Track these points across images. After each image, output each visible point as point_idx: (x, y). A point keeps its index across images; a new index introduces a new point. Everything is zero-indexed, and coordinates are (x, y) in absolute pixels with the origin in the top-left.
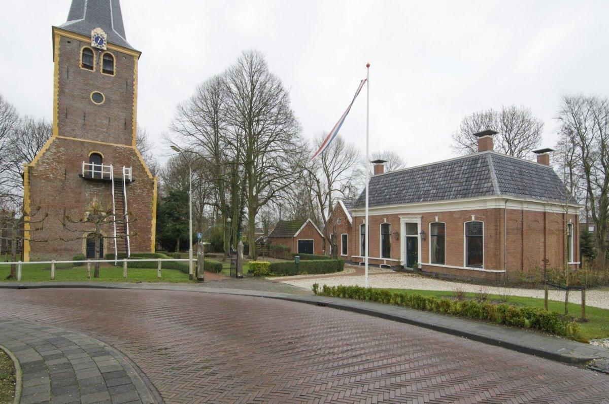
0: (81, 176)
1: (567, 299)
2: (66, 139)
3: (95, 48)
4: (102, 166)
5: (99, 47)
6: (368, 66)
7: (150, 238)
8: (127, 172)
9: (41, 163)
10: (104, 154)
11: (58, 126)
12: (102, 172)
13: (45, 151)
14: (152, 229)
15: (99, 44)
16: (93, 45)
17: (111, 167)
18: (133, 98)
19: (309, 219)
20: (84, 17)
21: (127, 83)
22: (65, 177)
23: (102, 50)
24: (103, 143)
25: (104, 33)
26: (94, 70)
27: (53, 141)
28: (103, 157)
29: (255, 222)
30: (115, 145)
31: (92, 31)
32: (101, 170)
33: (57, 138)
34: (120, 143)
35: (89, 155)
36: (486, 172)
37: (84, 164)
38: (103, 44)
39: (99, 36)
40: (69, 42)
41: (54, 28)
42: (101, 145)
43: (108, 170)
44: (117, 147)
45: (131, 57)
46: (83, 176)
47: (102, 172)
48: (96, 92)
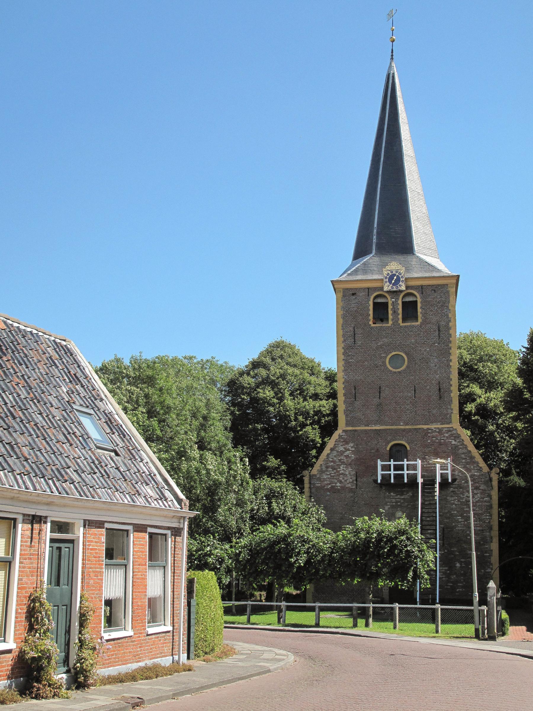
0: (376, 481)
2: (356, 431)
4: (405, 463)
5: (395, 289)
6: (390, 15)
8: (443, 467)
10: (409, 443)
13: (329, 452)
14: (492, 558)
15: (394, 284)
17: (419, 462)
21: (439, 327)
23: (401, 291)
24: (407, 427)
25: (400, 267)
26: (390, 322)
28: (408, 448)
29: (489, 586)
30: (425, 427)
32: (403, 470)
33: (343, 431)
35: (388, 449)
36: (300, 418)
37: (379, 463)
38: (401, 283)
41: (332, 282)
42: (404, 430)
43: (415, 468)
44: (428, 429)
46: (379, 481)
47: (406, 472)
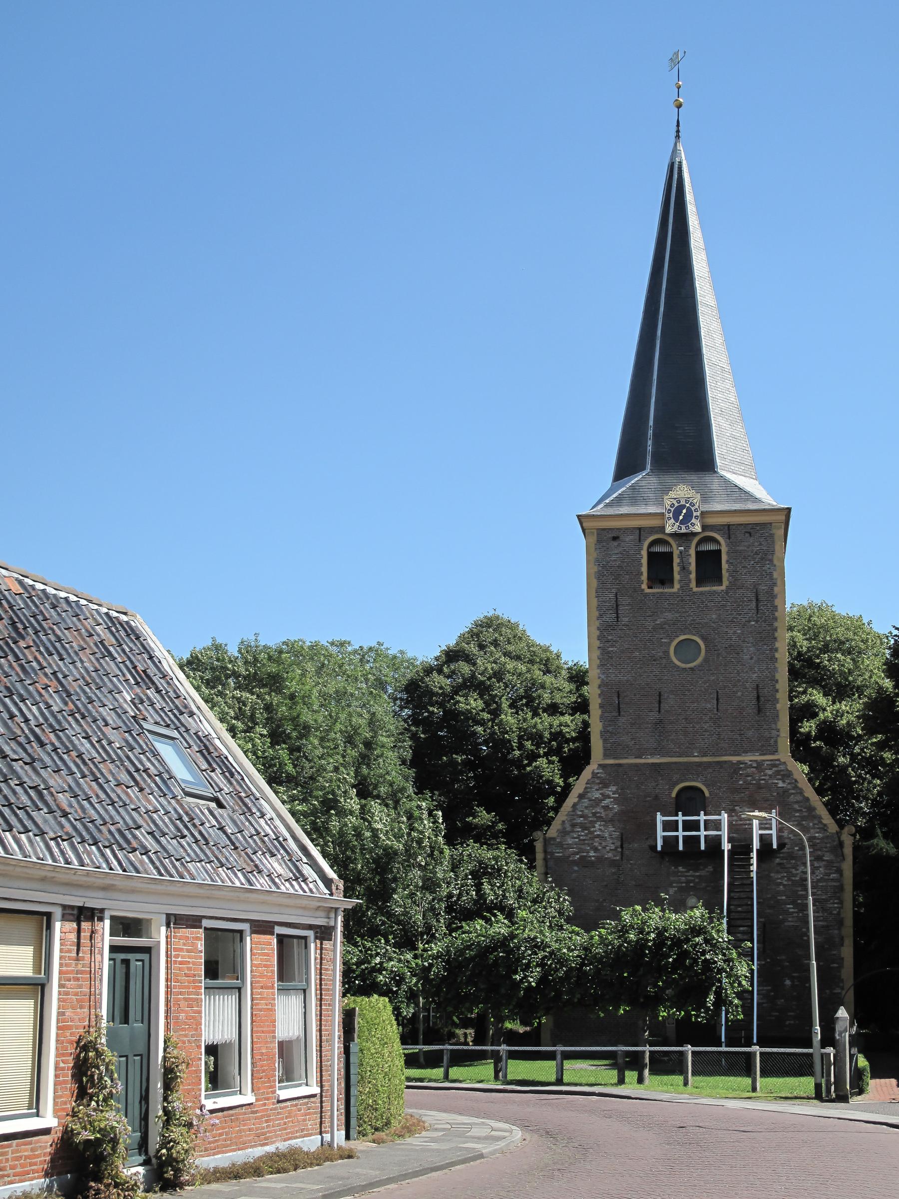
1: (79, 925)
3: (675, 535)
4: (702, 817)
5: (684, 531)
7: (605, 741)
9: (568, 828)
10: (707, 786)
11: (602, 736)
12: (703, 833)
13: (576, 800)
15: (682, 523)
16: (668, 530)
18: (776, 630)
19: (249, 1098)
20: (649, 467)
22: (622, 853)
24: (705, 759)
26: (677, 586)
27: (593, 773)
28: (707, 794)
30: (735, 759)
31: (666, 497)
33: (600, 765)
34: (746, 752)
35: (674, 795)
37: (660, 818)
38: (693, 520)
39: (683, 503)
40: (615, 538)
42: (700, 764)
43: (717, 825)
44: (740, 762)
45: (843, 959)
47: (703, 833)
48: (682, 637)
